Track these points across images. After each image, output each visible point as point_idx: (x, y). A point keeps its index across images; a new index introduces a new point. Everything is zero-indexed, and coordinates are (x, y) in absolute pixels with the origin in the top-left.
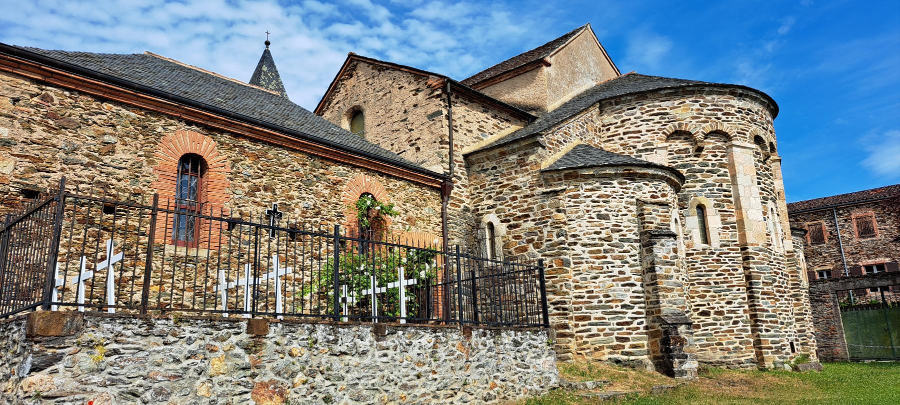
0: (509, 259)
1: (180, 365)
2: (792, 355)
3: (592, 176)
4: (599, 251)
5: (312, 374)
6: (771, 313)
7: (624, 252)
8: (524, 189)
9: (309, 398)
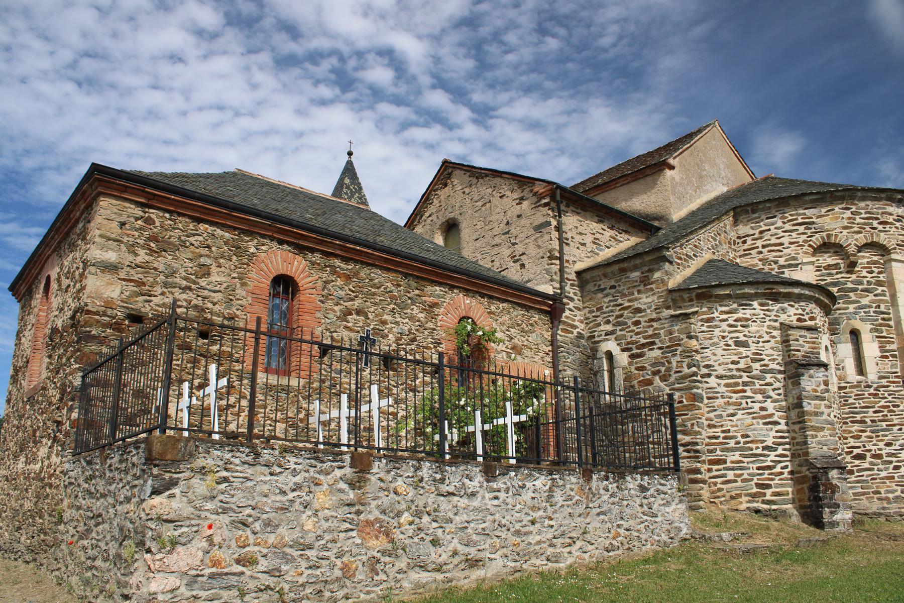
0: (631, 395)
1: (286, 498)
3: (728, 296)
4: (737, 384)
5: (418, 514)
7: (766, 384)
8: (648, 311)
9: (416, 540)
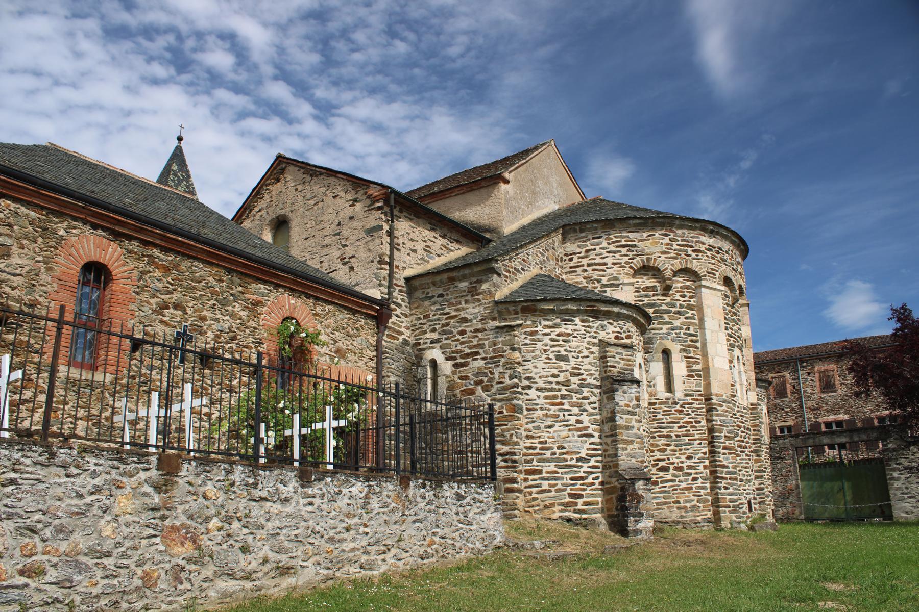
0: (453, 404)
1: (83, 501)
2: (749, 514)
3: (552, 311)
4: (556, 397)
5: (228, 520)
6: (731, 469)
7: (583, 398)
8: (474, 321)
9: (224, 546)
